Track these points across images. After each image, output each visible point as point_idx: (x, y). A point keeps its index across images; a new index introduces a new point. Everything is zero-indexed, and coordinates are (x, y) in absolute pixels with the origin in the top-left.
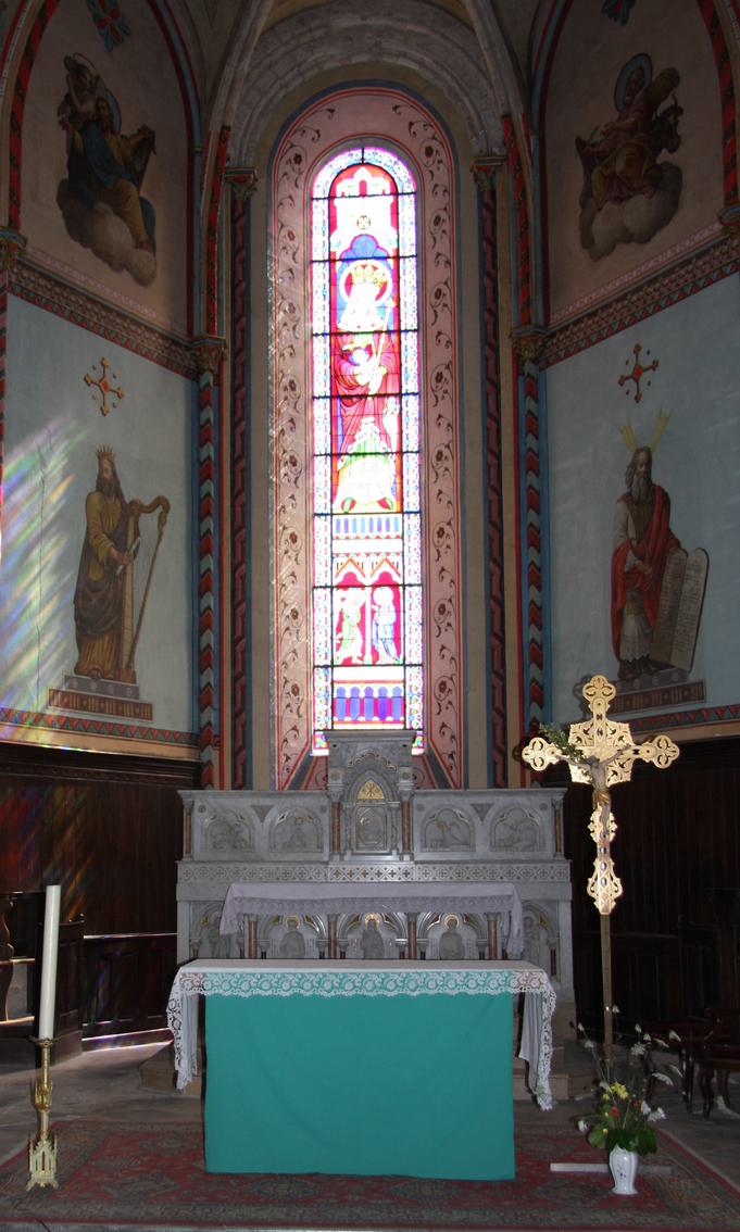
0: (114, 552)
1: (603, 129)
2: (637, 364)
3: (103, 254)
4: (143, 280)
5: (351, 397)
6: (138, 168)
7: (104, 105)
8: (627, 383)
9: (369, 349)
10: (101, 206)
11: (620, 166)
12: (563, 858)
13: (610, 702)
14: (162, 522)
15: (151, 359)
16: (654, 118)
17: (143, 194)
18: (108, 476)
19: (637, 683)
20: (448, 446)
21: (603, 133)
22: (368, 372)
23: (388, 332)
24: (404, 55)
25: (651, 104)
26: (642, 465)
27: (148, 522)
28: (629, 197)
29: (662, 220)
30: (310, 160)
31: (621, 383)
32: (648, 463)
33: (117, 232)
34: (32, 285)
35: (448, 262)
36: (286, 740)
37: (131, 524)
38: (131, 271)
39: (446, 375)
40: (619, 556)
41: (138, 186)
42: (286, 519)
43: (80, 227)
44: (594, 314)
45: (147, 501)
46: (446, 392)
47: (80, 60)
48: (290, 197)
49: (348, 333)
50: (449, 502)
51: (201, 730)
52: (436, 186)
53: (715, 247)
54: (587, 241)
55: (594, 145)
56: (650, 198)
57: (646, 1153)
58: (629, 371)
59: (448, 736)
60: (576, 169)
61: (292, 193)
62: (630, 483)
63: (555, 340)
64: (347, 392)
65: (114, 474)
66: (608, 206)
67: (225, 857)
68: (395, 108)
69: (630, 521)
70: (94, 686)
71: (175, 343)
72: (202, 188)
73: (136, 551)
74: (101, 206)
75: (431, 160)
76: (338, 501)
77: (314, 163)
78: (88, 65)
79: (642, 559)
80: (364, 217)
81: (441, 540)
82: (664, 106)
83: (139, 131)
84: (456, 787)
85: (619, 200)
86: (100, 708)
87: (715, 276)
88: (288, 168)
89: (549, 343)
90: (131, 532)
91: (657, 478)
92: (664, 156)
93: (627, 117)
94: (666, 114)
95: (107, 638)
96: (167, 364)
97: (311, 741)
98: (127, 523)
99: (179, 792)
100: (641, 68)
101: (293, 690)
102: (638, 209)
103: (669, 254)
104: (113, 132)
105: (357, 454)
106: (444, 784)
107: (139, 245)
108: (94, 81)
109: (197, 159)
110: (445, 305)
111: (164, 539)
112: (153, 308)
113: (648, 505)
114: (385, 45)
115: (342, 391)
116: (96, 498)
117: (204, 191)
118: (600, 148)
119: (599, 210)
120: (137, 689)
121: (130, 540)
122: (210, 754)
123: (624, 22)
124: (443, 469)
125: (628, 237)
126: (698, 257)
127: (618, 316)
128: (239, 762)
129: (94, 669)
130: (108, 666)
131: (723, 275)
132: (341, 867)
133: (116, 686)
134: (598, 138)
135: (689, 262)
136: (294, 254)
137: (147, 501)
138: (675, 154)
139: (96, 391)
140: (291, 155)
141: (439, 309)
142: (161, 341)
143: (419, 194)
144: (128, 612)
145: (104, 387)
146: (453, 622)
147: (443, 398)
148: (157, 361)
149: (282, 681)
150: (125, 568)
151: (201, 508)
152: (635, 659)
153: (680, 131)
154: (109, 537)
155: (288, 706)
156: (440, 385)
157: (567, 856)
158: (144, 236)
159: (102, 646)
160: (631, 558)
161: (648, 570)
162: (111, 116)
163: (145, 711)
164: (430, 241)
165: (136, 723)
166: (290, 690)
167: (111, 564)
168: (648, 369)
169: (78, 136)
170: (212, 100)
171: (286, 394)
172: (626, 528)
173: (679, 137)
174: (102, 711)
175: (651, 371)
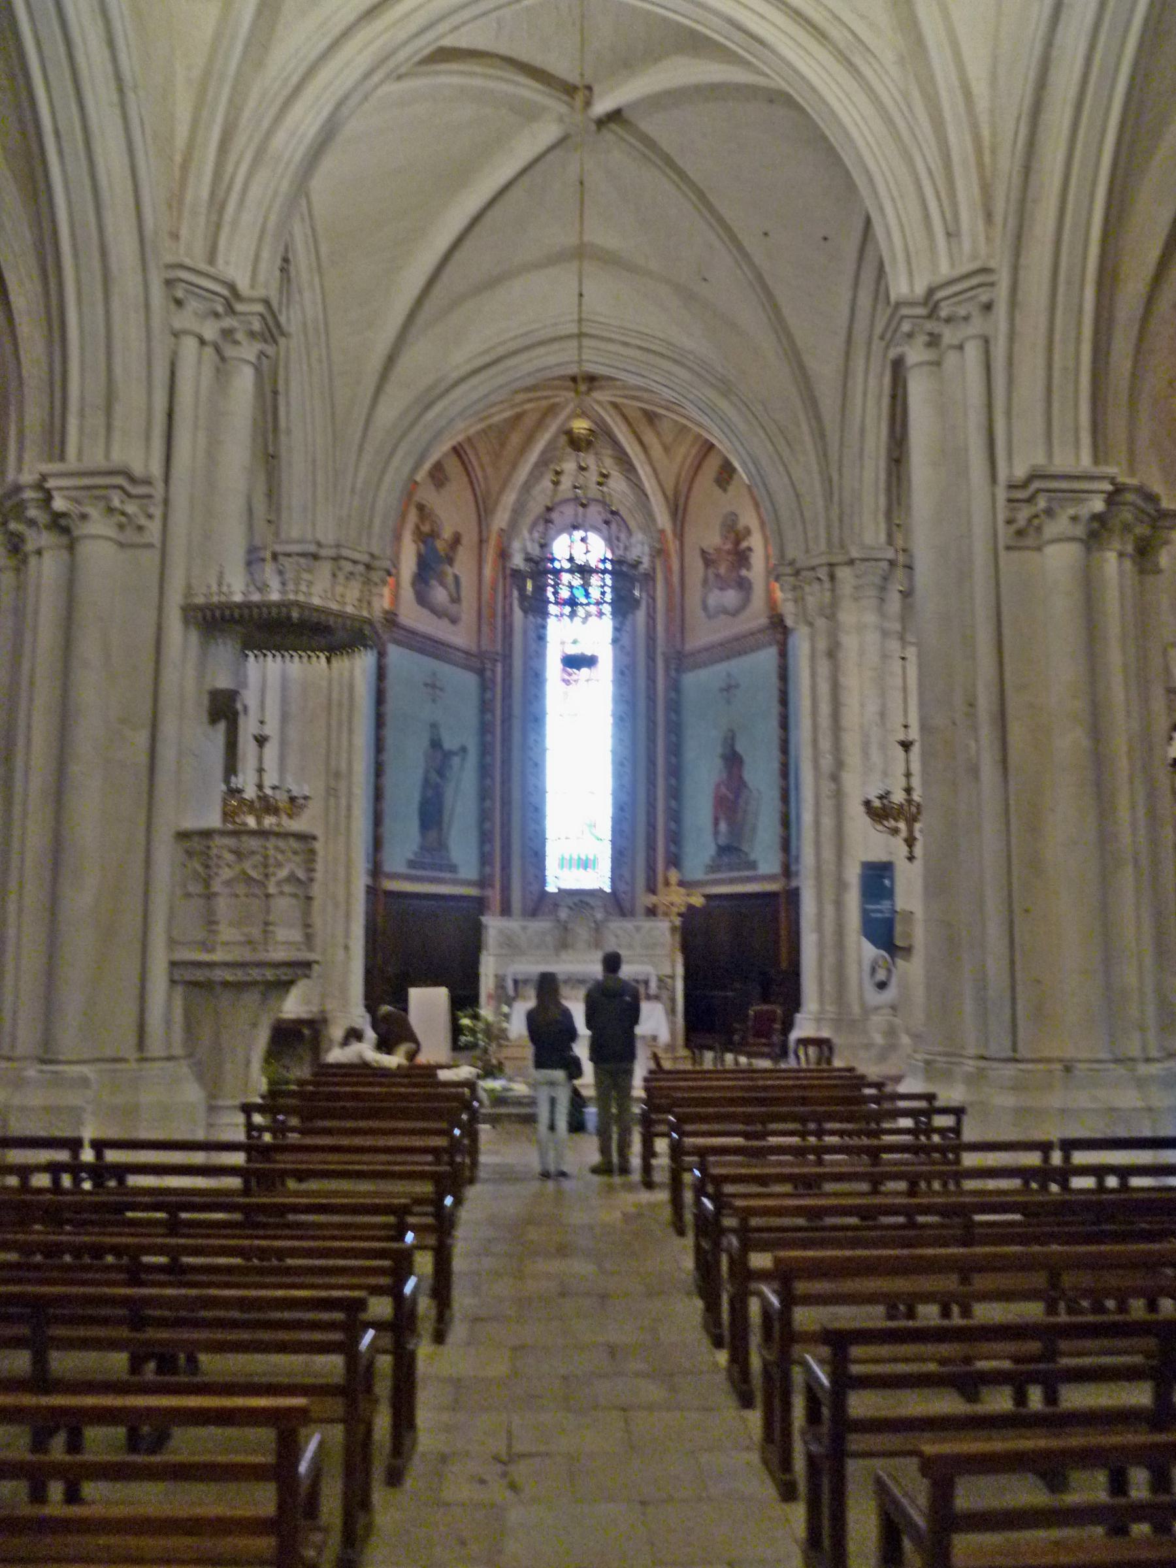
4: (454, 621)
25: (737, 542)
27: (456, 760)
32: (733, 738)
40: (718, 786)
43: (422, 599)
54: (705, 608)
57: (977, 1393)
60: (699, 564)
74: (434, 582)
85: (721, 589)
91: (739, 748)
113: (733, 760)
122: (489, 892)
151: (485, 750)
159: (433, 834)
160: (723, 790)
161: (731, 796)
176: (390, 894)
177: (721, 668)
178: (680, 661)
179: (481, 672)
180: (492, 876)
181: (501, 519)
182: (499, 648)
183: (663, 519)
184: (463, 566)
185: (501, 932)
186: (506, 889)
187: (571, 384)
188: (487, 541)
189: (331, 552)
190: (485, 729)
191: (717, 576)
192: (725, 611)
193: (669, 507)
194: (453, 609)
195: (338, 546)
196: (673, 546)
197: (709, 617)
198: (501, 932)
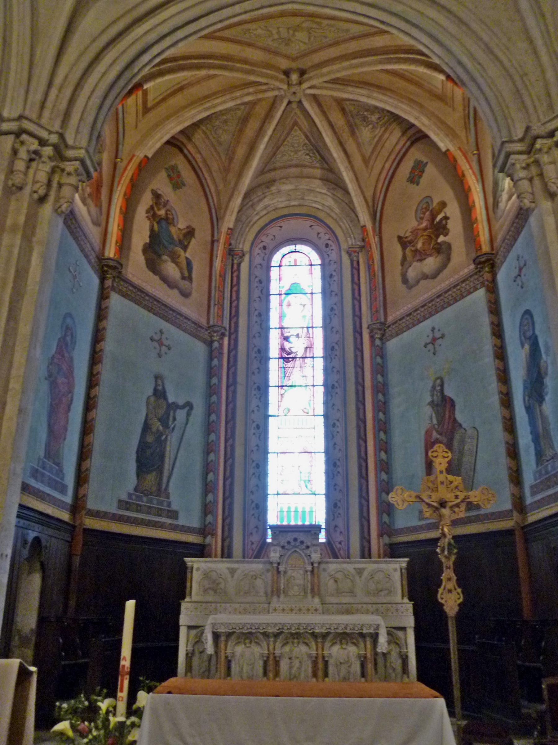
0: (161, 428)
1: (410, 230)
2: (433, 336)
3: (165, 279)
4: (186, 295)
5: (288, 358)
7: (170, 213)
8: (428, 346)
9: (298, 336)
10: (165, 257)
11: (419, 245)
12: (408, 601)
13: (448, 462)
14: (188, 415)
16: (435, 223)
17: (187, 255)
18: (160, 388)
21: (411, 232)
22: (297, 346)
23: (308, 328)
25: (433, 217)
26: (439, 385)
27: (181, 414)
28: (425, 259)
29: (444, 266)
31: (425, 346)
32: (442, 385)
33: (171, 270)
34: (125, 289)
36: (251, 534)
37: (172, 414)
39: (336, 347)
41: (185, 251)
43: (153, 265)
44: (410, 314)
45: (181, 402)
47: (159, 192)
49: (287, 328)
51: (205, 526)
52: (330, 261)
54: (405, 281)
55: (406, 238)
58: (429, 340)
60: (398, 248)
62: (432, 396)
63: (390, 329)
64: (287, 356)
65: (164, 388)
67: (210, 599)
69: (434, 415)
70: (145, 499)
72: (217, 257)
73: (173, 428)
74: (165, 257)
75: (328, 249)
76: (281, 409)
78: (163, 194)
79: (441, 434)
80: (296, 275)
81: (334, 429)
84: (342, 558)
85: (421, 260)
87: (472, 290)
89: (387, 331)
90: (171, 419)
91: (448, 392)
92: (441, 239)
93: (422, 223)
94: (441, 220)
97: (265, 536)
99: (185, 559)
100: (427, 202)
102: (431, 263)
103: (447, 282)
104: (174, 226)
105: (291, 386)
106: (336, 556)
107: (183, 278)
109: (216, 244)
110: (335, 314)
111: (190, 424)
114: (306, 198)
115: (285, 355)
116: (152, 399)
117: (218, 258)
119: (410, 266)
125: (425, 277)
127: (422, 314)
128: (226, 544)
129: (145, 490)
130: (154, 489)
131: (476, 289)
132: (277, 606)
133: (158, 500)
134: (407, 235)
135: (458, 285)
137: (181, 402)
139: (156, 344)
141: (332, 317)
143: (323, 265)
144: (167, 460)
145: (161, 344)
147: (335, 358)
149: (250, 502)
150: (166, 438)
153: (449, 226)
155: (253, 515)
157: (410, 599)
158: (186, 274)
159: (150, 479)
162: (173, 219)
163: (174, 515)
164: (327, 285)
165: (168, 521)
167: (159, 434)
168: (438, 339)
169: (156, 226)
170: (223, 218)
172: (431, 419)
174: (149, 513)
175: (441, 339)
176: (88, 532)
177: (427, 324)
178: (383, 331)
179: (210, 344)
180: (213, 525)
181: (229, 221)
182: (226, 323)
183: (364, 218)
184: (195, 252)
185: (206, 575)
186: (227, 537)
187: (283, 77)
188: (218, 241)
189: (13, 126)
190: (211, 390)
191: (416, 251)
192: (425, 277)
193: (370, 214)
194: (184, 284)
195: (21, 118)
196: (374, 241)
197: (410, 288)
198: (206, 575)
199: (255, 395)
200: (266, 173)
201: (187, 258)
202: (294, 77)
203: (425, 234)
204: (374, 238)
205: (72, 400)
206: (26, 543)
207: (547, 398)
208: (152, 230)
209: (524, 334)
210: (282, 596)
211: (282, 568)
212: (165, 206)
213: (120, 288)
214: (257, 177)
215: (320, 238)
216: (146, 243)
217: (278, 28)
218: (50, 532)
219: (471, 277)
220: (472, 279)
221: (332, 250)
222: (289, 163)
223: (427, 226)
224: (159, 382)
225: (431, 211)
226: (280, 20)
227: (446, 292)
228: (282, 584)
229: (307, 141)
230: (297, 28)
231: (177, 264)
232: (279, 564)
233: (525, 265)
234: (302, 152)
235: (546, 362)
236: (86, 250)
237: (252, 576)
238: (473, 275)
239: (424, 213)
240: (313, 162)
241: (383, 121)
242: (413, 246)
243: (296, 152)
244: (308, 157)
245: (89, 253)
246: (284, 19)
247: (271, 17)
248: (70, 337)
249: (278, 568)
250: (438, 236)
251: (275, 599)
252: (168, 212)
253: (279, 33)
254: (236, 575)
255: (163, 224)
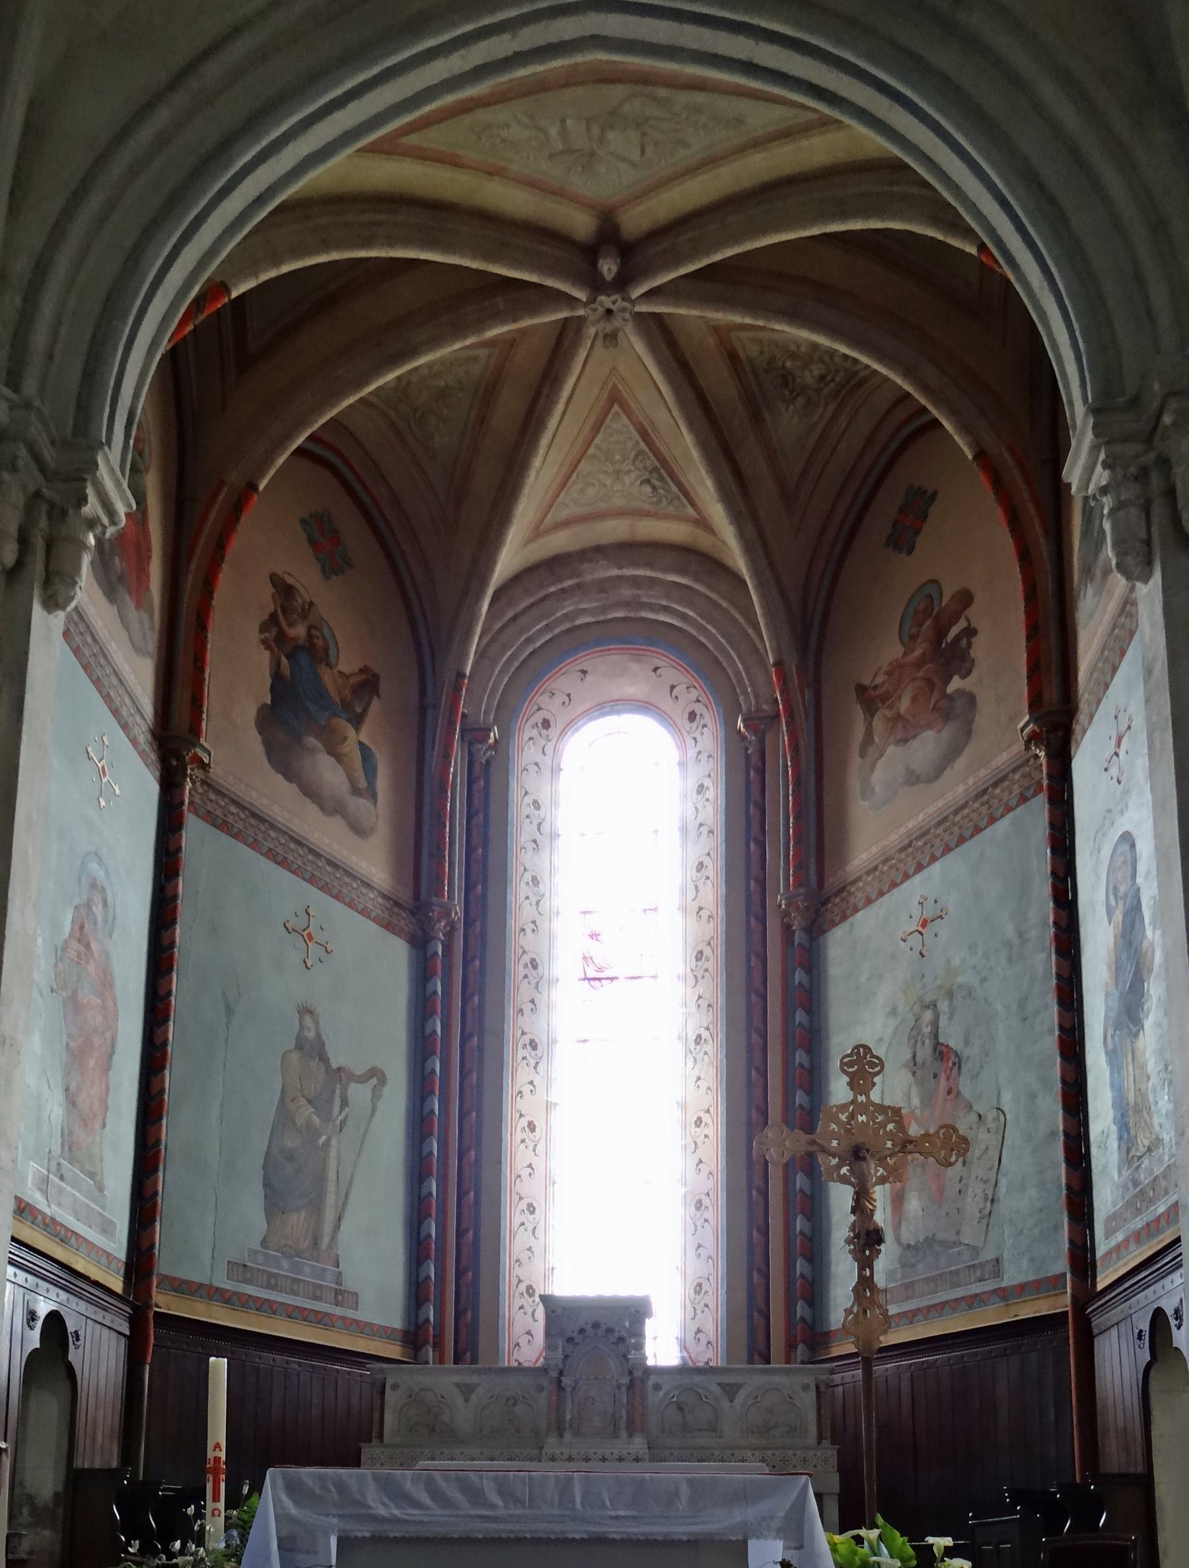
0: (316, 1120)
3: (310, 791)
4: (359, 830)
6: (359, 710)
10: (311, 741)
11: (904, 705)
15: (368, 916)
17: (363, 737)
18: (311, 1035)
19: (920, 1266)
20: (707, 1028)
24: (666, 609)
27: (359, 1093)
30: (560, 728)
33: (329, 773)
35: (711, 832)
38: (345, 817)
41: (357, 730)
42: (521, 1104)
43: (283, 757)
45: (359, 1071)
46: (706, 970)
47: (290, 580)
48: (537, 764)
50: (709, 1088)
53: (1014, 771)
55: (876, 687)
56: (939, 732)
59: (704, 1342)
61: (538, 760)
65: (318, 1035)
66: (891, 750)
68: (655, 670)
69: (914, 1090)
70: (285, 1264)
71: (396, 904)
73: (343, 1123)
77: (563, 732)
78: (298, 586)
82: (954, 631)
83: (361, 670)
86: (292, 1289)
87: (1013, 803)
88: (535, 732)
92: (956, 684)
94: (957, 638)
95: (303, 1214)
96: (388, 926)
98: (334, 1092)
100: (930, 596)
101: (527, 1291)
104: (329, 665)
107: (356, 791)
108: (307, 606)
109: (430, 712)
111: (378, 1115)
112: (373, 863)
116: (295, 1057)
118: (883, 689)
119: (881, 756)
120: (340, 1274)
121: (336, 1109)
123: (910, 552)
124: (702, 1053)
126: (995, 785)
129: (286, 1245)
130: (304, 1244)
134: (880, 680)
136: (540, 824)
138: (969, 679)
140: (538, 718)
142: (380, 900)
146: (710, 1218)
148: (376, 920)
149: (515, 1281)
150: (328, 1141)
152: (918, 1242)
154: (309, 1101)
156: (700, 963)
158: (363, 783)
162: (327, 650)
163: (342, 1296)
166: (524, 1290)
167: (311, 1132)
169: (284, 660)
171: (526, 971)
173: (973, 661)
199: (524, 1058)
200: (547, 531)
201: (361, 744)
202: (608, 267)
203: (921, 674)
204: (803, 696)
205: (113, 1045)
206: (33, 1320)
207: (1148, 1023)
208: (277, 676)
209: (1116, 889)
210: (568, 1435)
211: (567, 1381)
212: (304, 614)
213: (209, 807)
214: (525, 545)
215: (677, 697)
216: (264, 706)
217: (563, 121)
218: (82, 1306)
219: (1014, 771)
220: (1017, 776)
221: (704, 726)
222: (603, 506)
223: (924, 654)
224: (308, 1020)
225: (937, 617)
226: (568, 94)
227: (956, 812)
228: (568, 1412)
229: (643, 445)
230: (613, 119)
231: (339, 757)
232: (561, 1373)
233: (1129, 727)
234: (633, 475)
235: (1152, 944)
236: (124, 712)
237: (508, 1399)
238: (1021, 766)
239: (920, 625)
240: (659, 502)
241: (832, 385)
242: (890, 707)
243: (618, 475)
244: (647, 489)
245: (130, 720)
246: (580, 91)
247: (542, 86)
248: (101, 906)
249: (560, 1381)
250: (947, 680)
251: (552, 1440)
252: (314, 632)
253: (564, 133)
254: (474, 1397)
255: (304, 659)
